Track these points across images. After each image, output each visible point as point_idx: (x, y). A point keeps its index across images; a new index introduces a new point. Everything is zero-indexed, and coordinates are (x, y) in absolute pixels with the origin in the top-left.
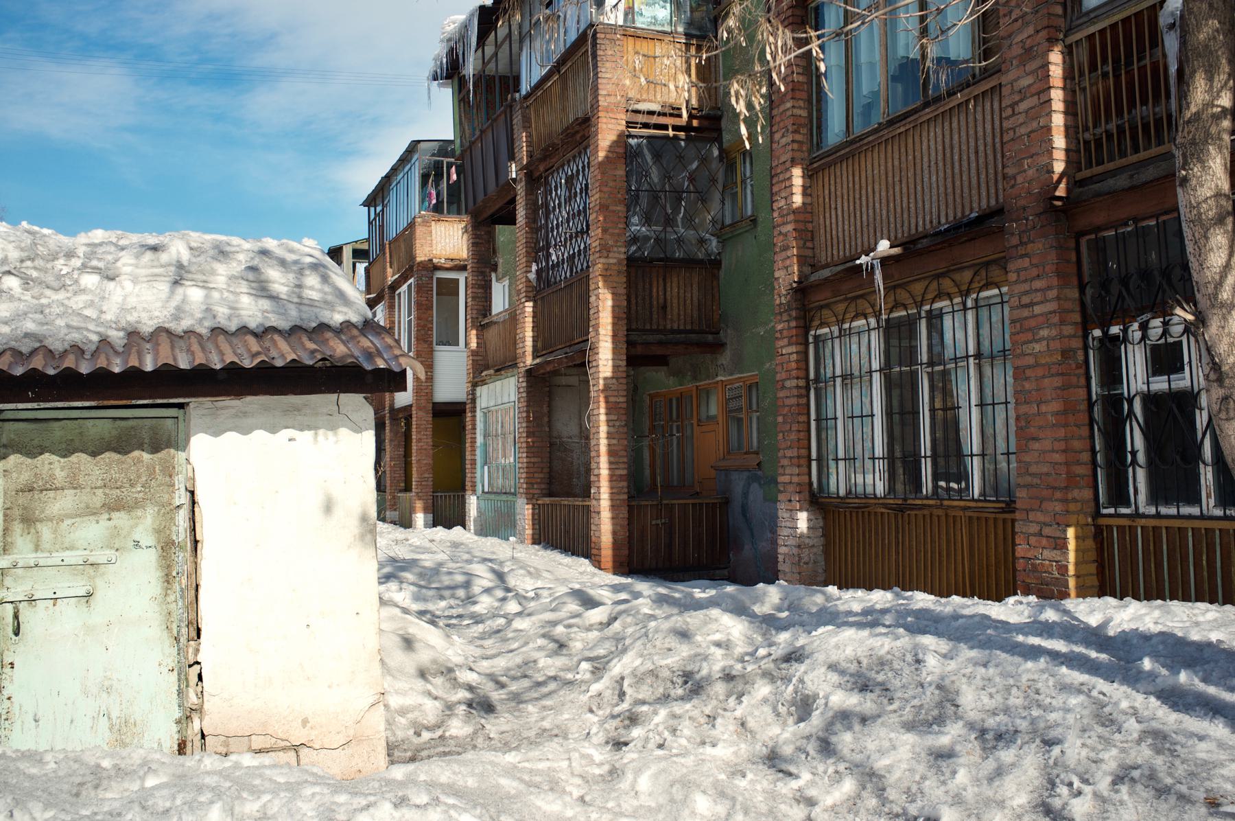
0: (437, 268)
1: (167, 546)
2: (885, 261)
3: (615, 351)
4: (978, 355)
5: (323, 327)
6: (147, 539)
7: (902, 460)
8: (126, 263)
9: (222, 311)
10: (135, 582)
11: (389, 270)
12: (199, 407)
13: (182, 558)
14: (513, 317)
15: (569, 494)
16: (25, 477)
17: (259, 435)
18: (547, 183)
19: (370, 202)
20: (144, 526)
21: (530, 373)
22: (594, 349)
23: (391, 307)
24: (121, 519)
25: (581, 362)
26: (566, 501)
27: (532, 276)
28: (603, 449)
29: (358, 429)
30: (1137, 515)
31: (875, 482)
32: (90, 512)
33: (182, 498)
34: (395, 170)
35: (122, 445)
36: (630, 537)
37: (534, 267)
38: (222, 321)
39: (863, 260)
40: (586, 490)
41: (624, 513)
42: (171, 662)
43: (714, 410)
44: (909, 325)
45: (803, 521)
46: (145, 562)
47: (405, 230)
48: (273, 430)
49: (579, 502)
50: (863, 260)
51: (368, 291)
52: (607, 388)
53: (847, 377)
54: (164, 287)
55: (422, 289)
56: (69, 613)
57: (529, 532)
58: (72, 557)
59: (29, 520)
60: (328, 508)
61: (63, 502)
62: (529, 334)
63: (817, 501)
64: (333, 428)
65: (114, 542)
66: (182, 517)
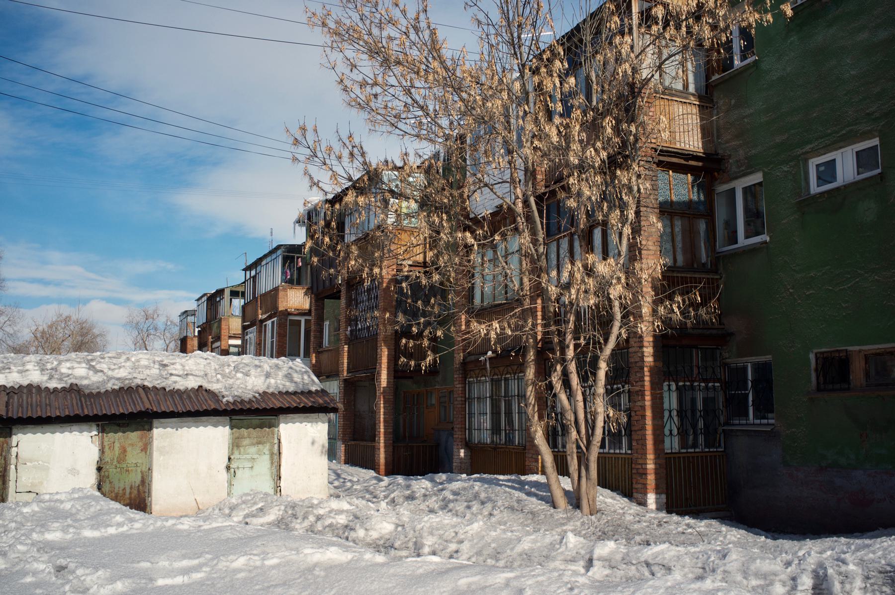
0: (290, 314)
1: (272, 454)
2: (490, 359)
3: (388, 375)
4: (518, 396)
5: (310, 392)
6: (267, 452)
7: (496, 429)
8: (253, 372)
9: (281, 387)
10: (264, 464)
11: (260, 311)
12: (281, 417)
13: (276, 457)
14: (337, 353)
15: (362, 440)
16: (237, 435)
17: (298, 424)
18: (357, 289)
19: (248, 269)
20: (266, 449)
21: (345, 380)
22: (379, 374)
23: (260, 332)
24: (260, 446)
25: (373, 377)
26: (362, 443)
27: (348, 333)
28: (382, 420)
29: (323, 423)
30: (559, 451)
31: (486, 437)
32: (253, 444)
33: (276, 441)
34: (265, 256)
35: (261, 426)
36: (393, 460)
37: (349, 329)
38: (281, 390)
39: (482, 358)
40: (373, 438)
41: (391, 449)
42: (272, 486)
43: (434, 402)
44: (499, 381)
45: (462, 453)
46: (267, 457)
47: (271, 291)
48: (301, 423)
49: (369, 444)
50: (482, 358)
51: (244, 321)
52: (384, 392)
53: (479, 398)
54: (263, 378)
55: (281, 326)
56: (247, 471)
57: (343, 458)
58: (248, 457)
59: (238, 446)
60: (313, 443)
61: (246, 442)
62: (346, 361)
63: (468, 445)
64: (317, 422)
65: (259, 453)
66: (276, 447)
